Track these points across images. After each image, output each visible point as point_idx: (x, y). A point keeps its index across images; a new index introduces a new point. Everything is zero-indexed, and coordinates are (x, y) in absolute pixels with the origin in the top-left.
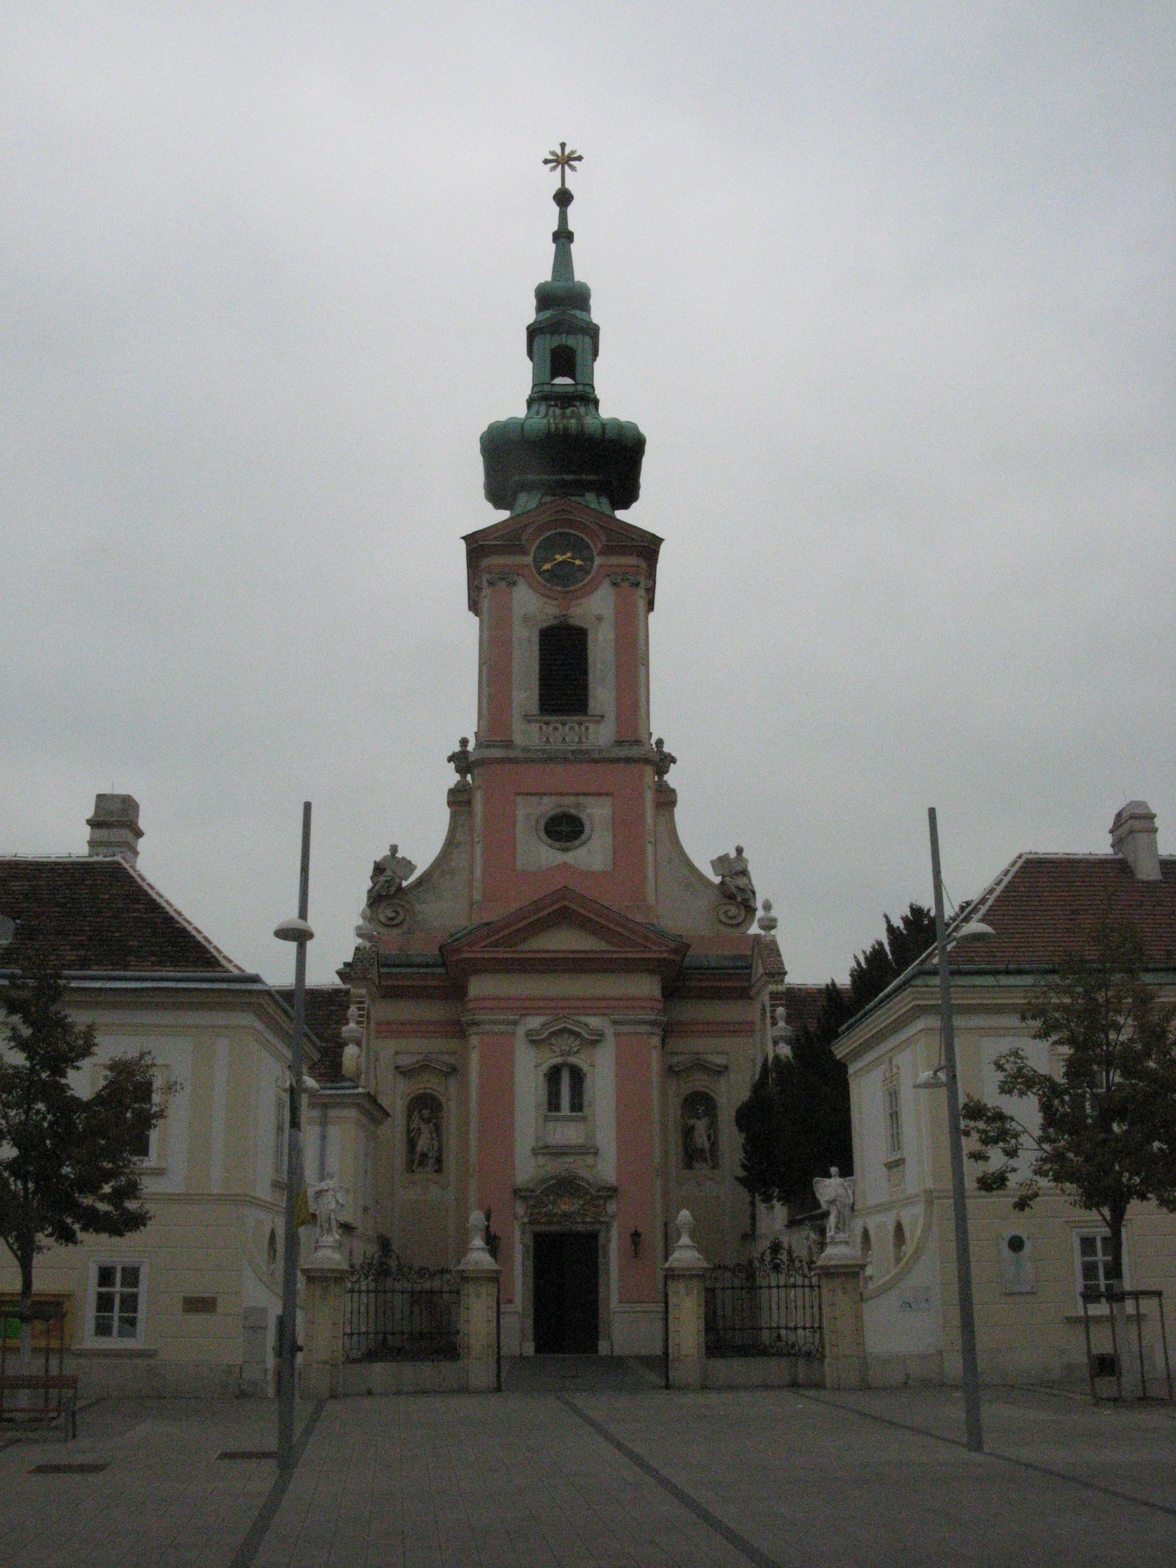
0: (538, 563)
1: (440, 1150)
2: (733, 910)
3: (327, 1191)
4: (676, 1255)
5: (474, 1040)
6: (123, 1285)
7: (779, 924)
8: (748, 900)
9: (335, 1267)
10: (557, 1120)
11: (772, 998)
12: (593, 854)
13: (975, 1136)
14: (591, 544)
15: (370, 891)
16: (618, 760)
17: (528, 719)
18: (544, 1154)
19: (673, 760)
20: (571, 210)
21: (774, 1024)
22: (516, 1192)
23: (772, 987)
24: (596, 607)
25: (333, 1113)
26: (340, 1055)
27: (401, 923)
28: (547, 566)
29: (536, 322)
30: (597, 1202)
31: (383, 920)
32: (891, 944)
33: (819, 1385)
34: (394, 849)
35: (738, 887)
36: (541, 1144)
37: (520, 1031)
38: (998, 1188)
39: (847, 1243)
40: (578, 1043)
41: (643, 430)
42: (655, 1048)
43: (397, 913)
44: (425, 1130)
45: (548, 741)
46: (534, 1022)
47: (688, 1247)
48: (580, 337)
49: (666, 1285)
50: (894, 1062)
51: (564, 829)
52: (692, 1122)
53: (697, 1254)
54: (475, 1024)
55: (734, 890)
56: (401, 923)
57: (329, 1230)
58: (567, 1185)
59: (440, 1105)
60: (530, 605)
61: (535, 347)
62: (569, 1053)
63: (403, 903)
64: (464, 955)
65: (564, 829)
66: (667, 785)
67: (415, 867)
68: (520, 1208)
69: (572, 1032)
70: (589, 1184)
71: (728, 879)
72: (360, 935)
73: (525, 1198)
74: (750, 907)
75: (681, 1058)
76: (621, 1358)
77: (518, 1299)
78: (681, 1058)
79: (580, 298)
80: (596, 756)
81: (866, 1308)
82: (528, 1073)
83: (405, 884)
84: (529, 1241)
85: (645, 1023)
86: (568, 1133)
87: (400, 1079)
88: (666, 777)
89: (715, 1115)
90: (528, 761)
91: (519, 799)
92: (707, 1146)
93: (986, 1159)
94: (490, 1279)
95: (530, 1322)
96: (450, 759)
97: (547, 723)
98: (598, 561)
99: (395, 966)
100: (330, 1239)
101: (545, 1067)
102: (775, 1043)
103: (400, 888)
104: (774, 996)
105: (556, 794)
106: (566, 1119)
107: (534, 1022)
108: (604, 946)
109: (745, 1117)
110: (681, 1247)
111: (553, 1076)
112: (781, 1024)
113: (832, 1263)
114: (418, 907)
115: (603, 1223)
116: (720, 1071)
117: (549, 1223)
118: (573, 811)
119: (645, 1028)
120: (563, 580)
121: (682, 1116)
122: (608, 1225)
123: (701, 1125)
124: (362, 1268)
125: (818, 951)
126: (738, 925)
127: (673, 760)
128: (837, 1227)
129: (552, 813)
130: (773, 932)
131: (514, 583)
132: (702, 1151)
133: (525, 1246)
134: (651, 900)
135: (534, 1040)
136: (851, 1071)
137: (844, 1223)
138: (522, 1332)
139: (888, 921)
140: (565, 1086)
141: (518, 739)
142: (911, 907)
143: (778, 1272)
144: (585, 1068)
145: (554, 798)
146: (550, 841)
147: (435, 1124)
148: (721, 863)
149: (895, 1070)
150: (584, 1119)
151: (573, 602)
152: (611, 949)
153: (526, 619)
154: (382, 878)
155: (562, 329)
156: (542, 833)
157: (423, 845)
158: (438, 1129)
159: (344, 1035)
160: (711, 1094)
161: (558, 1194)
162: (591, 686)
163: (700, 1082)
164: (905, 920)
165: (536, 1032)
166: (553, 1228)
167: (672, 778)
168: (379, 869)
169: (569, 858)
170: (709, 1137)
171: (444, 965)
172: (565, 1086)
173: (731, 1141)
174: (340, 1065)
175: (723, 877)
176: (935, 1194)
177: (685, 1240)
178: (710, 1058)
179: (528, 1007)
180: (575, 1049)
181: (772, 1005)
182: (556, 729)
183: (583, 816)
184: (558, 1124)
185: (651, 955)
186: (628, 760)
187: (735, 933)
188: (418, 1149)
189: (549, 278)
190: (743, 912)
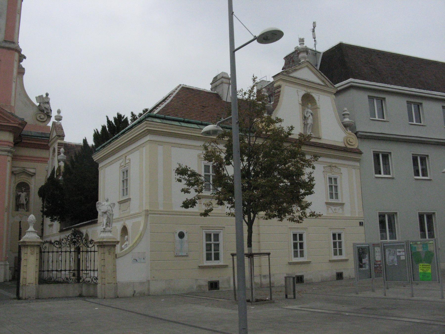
2: (43, 116)
4: (27, 235)
6: (390, 239)
7: (63, 119)
8: (48, 113)
11: (58, 145)
13: (184, 182)
19: (25, 58)
21: (59, 153)
23: (59, 141)
32: (115, 122)
33: (94, 296)
35: (45, 108)
38: (191, 206)
39: (111, 231)
42: (9, 161)
50: (127, 158)
52: (19, 193)
55: (44, 108)
66: (22, 66)
75: (17, 169)
78: (17, 169)
81: (119, 262)
85: (5, 151)
88: (21, 63)
92: (25, 203)
93: (189, 192)
102: (59, 161)
104: (60, 145)
109: (42, 192)
110: (29, 232)
112: (62, 154)
113: (105, 240)
116: (32, 175)
119: (6, 153)
123: (23, 195)
125: (79, 130)
126: (44, 122)
127: (25, 58)
128: (107, 224)
130: (60, 122)
132: (23, 204)
134: (13, 104)
136: (100, 166)
137: (110, 223)
139: (108, 119)
142: (118, 114)
148: (40, 98)
149: (127, 161)
160: (29, 184)
163: (23, 178)
164: (115, 119)
167: (24, 64)
170: (26, 200)
173: (36, 201)
175: (40, 103)
176: (149, 212)
177: (31, 228)
178: (28, 170)
181: (58, 148)
185: (11, 125)
186: (9, 49)
187: (41, 124)
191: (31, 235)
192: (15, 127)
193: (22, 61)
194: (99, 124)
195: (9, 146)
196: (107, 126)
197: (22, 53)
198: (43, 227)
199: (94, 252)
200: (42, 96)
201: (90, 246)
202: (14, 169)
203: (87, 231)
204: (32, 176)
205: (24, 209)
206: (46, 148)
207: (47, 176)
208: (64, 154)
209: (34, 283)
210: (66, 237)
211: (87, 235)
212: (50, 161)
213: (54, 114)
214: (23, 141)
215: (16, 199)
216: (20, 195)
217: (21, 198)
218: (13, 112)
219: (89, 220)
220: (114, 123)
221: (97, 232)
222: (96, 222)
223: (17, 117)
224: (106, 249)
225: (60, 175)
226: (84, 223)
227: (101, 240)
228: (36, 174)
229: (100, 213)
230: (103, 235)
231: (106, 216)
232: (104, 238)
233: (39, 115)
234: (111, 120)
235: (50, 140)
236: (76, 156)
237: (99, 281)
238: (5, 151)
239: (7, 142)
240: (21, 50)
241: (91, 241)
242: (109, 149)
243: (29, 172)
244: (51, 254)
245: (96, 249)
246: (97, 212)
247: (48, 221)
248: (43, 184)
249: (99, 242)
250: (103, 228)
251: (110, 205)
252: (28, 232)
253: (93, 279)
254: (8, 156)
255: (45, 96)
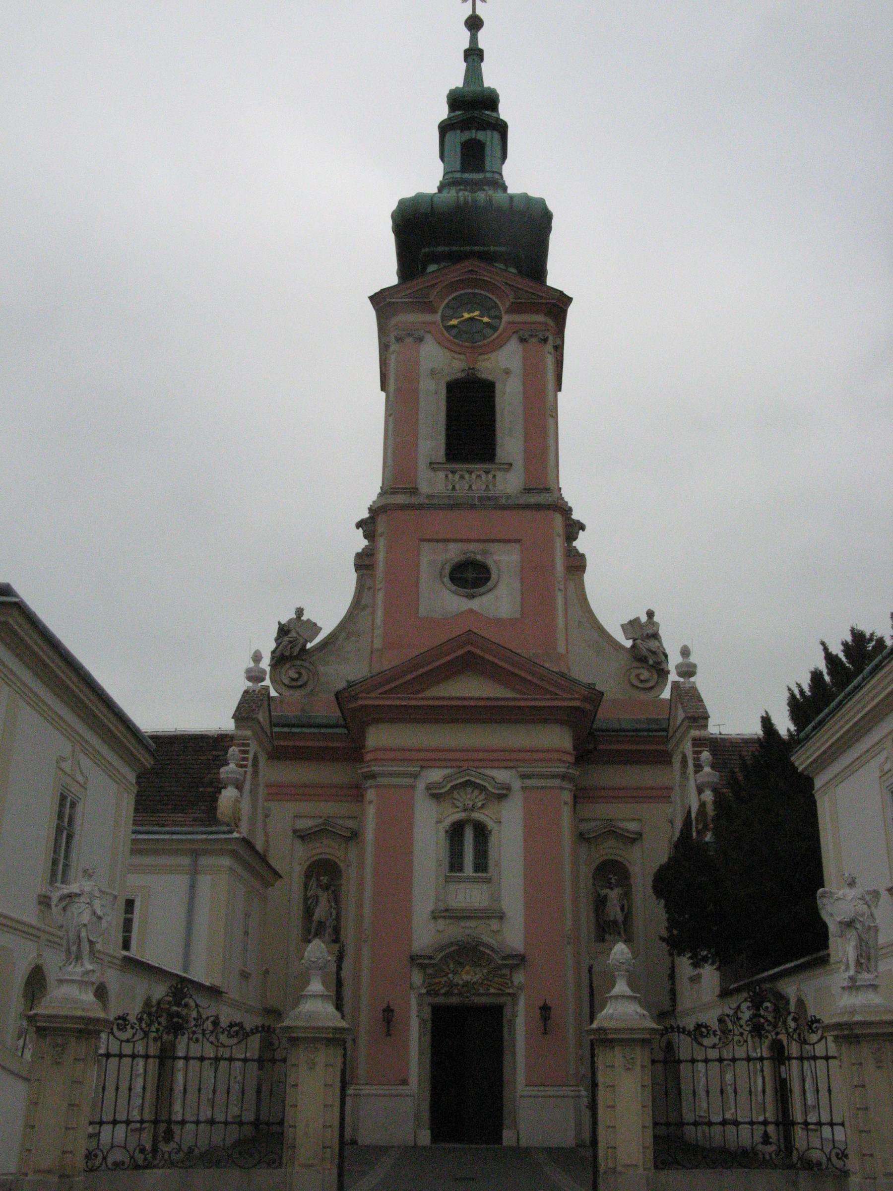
0: (444, 318)
1: (338, 918)
2: (645, 674)
3: (79, 895)
4: (608, 1010)
5: (371, 795)
7: (699, 671)
8: (659, 663)
9: (79, 1013)
10: (460, 880)
11: (694, 745)
12: (500, 602)
14: (500, 304)
15: (273, 652)
16: (527, 507)
17: (433, 466)
18: (444, 917)
19: (582, 527)
20: (481, 34)
21: (698, 767)
22: (412, 958)
24: (505, 363)
25: (204, 861)
26: (215, 800)
27: (305, 684)
28: (454, 322)
29: (449, 119)
30: (504, 971)
31: (286, 681)
32: (847, 656)
34: (300, 612)
36: (442, 906)
37: (421, 785)
39: (874, 987)
40: (482, 796)
41: (551, 207)
42: (566, 803)
43: (300, 674)
44: (324, 898)
45: (454, 488)
46: (436, 775)
47: (623, 997)
48: (489, 132)
49: (593, 1055)
51: (470, 576)
53: (640, 1010)
54: (373, 776)
55: (645, 652)
56: (305, 684)
57: (78, 958)
58: (468, 952)
59: (340, 871)
60: (437, 361)
61: (446, 154)
62: (473, 809)
63: (307, 664)
64: (360, 702)
65: (470, 576)
67: (321, 629)
68: (417, 978)
69: (476, 786)
70: (493, 950)
71: (639, 642)
72: (249, 678)
73: (422, 967)
74: (663, 670)
75: (592, 824)
76: (528, 1150)
77: (414, 1080)
78: (592, 824)
79: (490, 101)
80: (504, 501)
82: (428, 828)
83: (309, 646)
84: (427, 1012)
85: (553, 776)
86: (469, 895)
87: (298, 844)
88: (575, 544)
89: (629, 886)
90: (433, 507)
91: (426, 547)
92: (620, 918)
94: (329, 1042)
95: (426, 1106)
96: (359, 525)
97: (453, 472)
98: (506, 318)
99: (293, 726)
100: (79, 969)
101: (447, 823)
102: (700, 791)
103: (303, 649)
104: (699, 743)
105: (461, 541)
106: (469, 880)
107: (436, 775)
108: (509, 694)
109: (663, 883)
111: (456, 832)
112: (707, 769)
113: (858, 1018)
114: (322, 669)
115: (509, 994)
116: (635, 838)
117: (448, 994)
118: (479, 557)
119: (557, 782)
120: (470, 339)
121: (594, 884)
122: (513, 996)
123: (614, 895)
124: (140, 1020)
126: (651, 688)
127: (582, 527)
128: (858, 964)
129: (457, 559)
130: (692, 679)
131: (420, 339)
132: (615, 922)
133: (423, 1021)
134: (561, 649)
135: (436, 795)
136: (818, 783)
137: (869, 959)
138: (417, 1117)
139: (826, 649)
140: (468, 844)
141: (425, 488)
142: (853, 631)
143: (760, 1036)
144: (491, 825)
145: (459, 545)
146: (454, 588)
147: (333, 892)
148: (632, 626)
150: (488, 881)
151: (480, 358)
152: (518, 696)
153: (433, 373)
154: (286, 639)
155: (473, 123)
156: (447, 580)
157: (328, 611)
158: (336, 899)
159: (222, 776)
161: (460, 963)
162: (499, 434)
163: (610, 850)
165: (439, 785)
166: (454, 1000)
167: (581, 543)
168: (283, 630)
169: (475, 604)
170: (622, 909)
171: (345, 727)
172: (468, 844)
173: (650, 913)
174: (215, 808)
175: (635, 640)
177: (621, 987)
178: (620, 824)
179: (431, 758)
180: (479, 804)
181: (695, 752)
182: (462, 477)
183: (490, 562)
184: (462, 885)
186: (539, 507)
187: (642, 696)
188: (316, 917)
189: (461, 85)
190: (656, 676)
191: (623, 1010)
192: (576, 708)
193: (575, 538)
194: (802, 667)
195: (560, 760)
196: (825, 671)
197: (575, 516)
198: (673, 984)
199: (827, 1058)
200: (637, 620)
201: (814, 1038)
202: (585, 826)
203: (799, 990)
204: (634, 840)
205: (619, 933)
206: (663, 758)
207: (671, 838)
208: (712, 767)
209: (641, 1163)
210: (731, 1012)
211: (801, 1003)
212: (676, 796)
213: (674, 660)
214: (600, 747)
215: (596, 910)
216: (605, 897)
217: (608, 904)
218: (566, 671)
219: (802, 956)
220: (844, 659)
221: (833, 993)
222: (824, 961)
223: (574, 681)
224: (866, 1050)
225: (706, 827)
226: (788, 965)
227: (845, 1019)
228: (644, 836)
229: (832, 928)
230: (848, 1000)
231: (852, 935)
232: (853, 1012)
233: (637, 671)
234: (834, 653)
235: (671, 734)
236: (744, 766)
237: (853, 1163)
238: (553, 776)
239: (558, 751)
240: (570, 509)
241: (813, 1022)
242: (834, 730)
243: (622, 829)
244: (701, 1066)
245: (833, 1050)
246: (825, 926)
247: (684, 964)
248: (664, 859)
249: (839, 1026)
250: (846, 975)
251: (862, 899)
252: (611, 997)
253: (834, 1159)
254: (562, 788)
255: (644, 619)
